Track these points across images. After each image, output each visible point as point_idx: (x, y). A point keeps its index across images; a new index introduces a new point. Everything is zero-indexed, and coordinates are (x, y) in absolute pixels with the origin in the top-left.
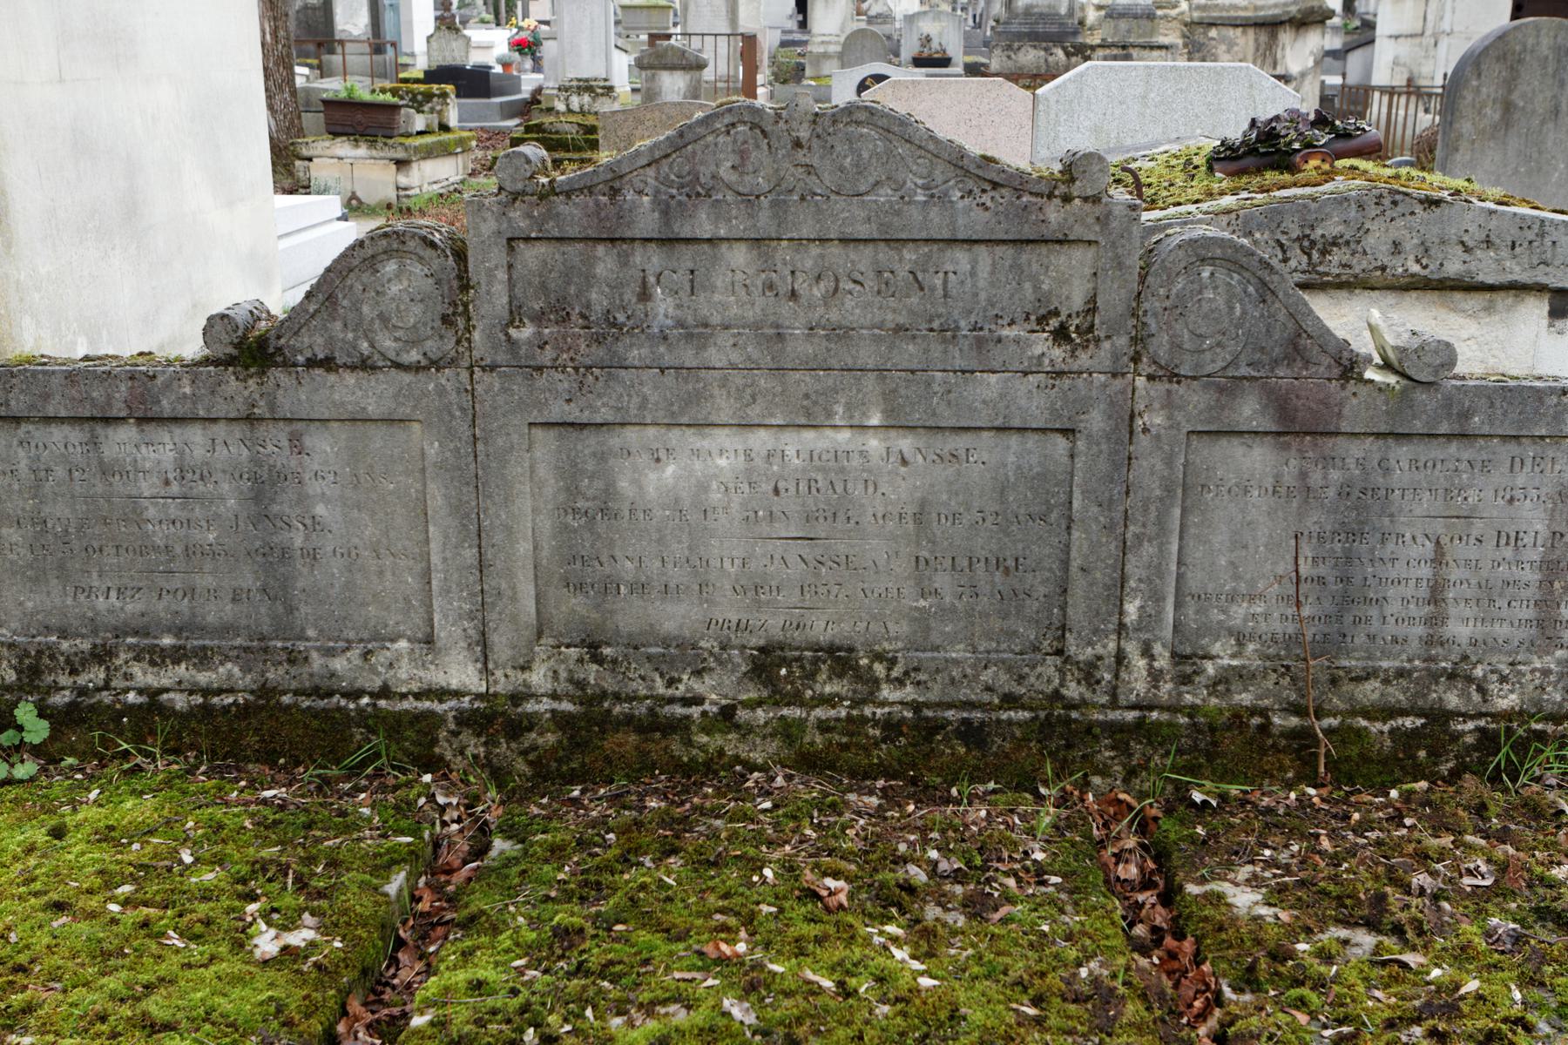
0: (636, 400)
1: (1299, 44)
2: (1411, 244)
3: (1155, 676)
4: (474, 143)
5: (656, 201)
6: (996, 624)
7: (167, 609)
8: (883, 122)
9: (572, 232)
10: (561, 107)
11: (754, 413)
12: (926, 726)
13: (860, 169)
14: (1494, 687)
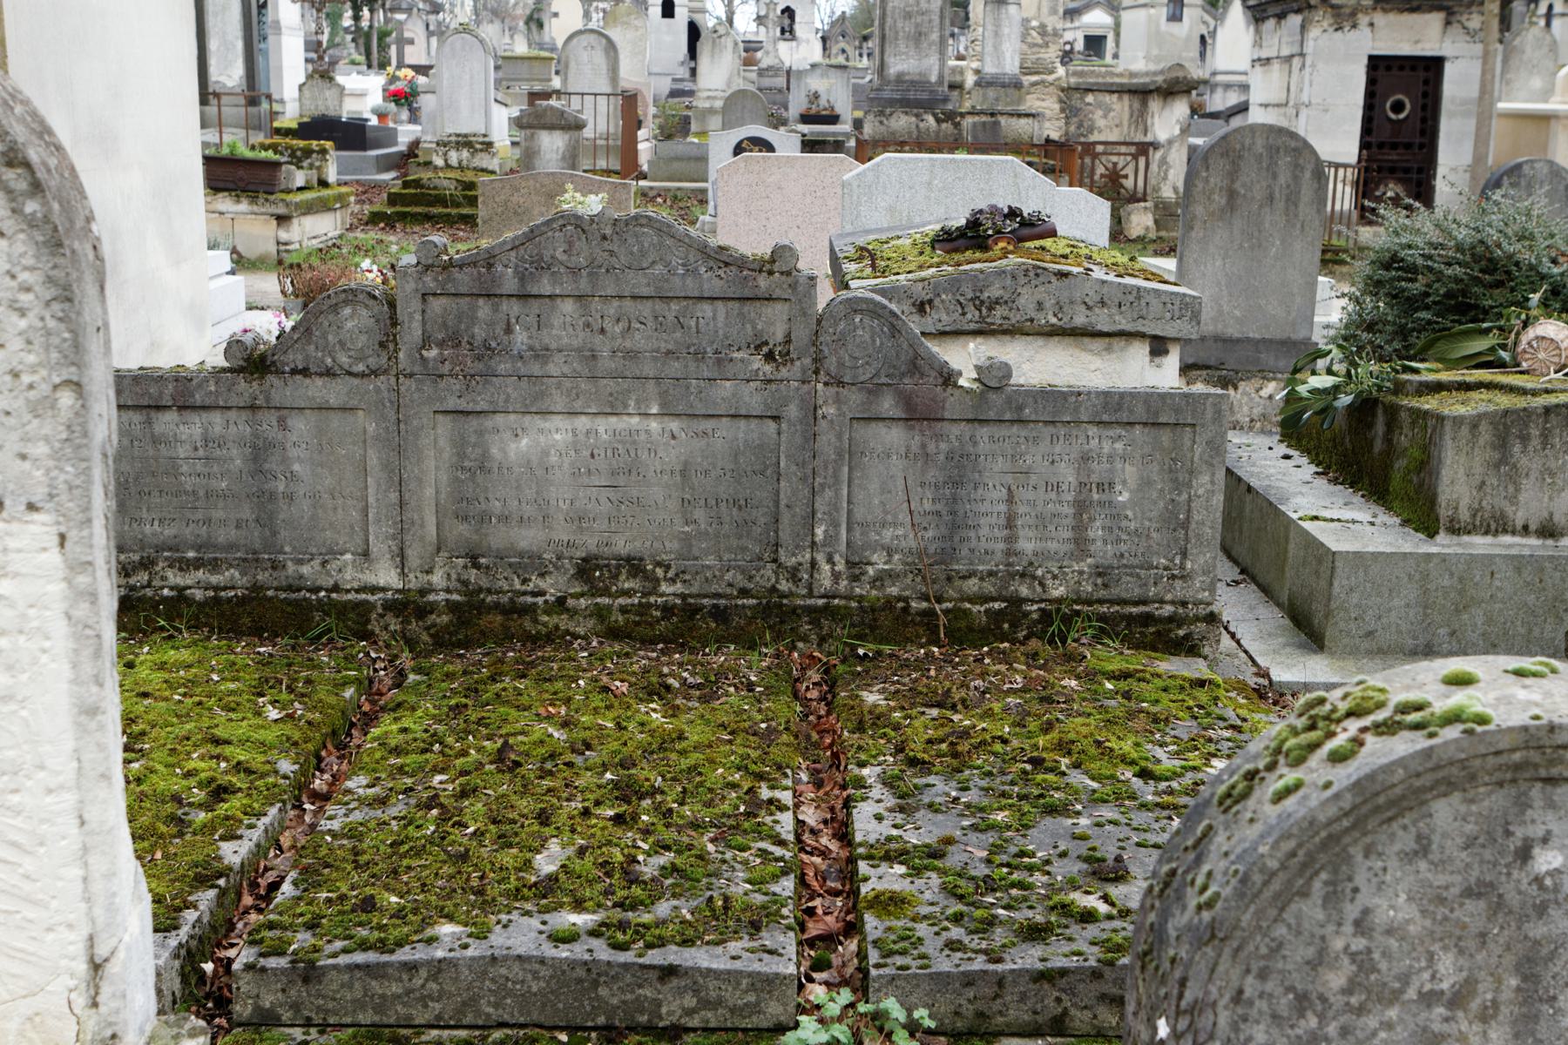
0: (503, 397)
1: (1166, 113)
2: (1049, 303)
3: (836, 576)
4: (352, 199)
5: (516, 272)
6: (735, 542)
7: (192, 533)
8: (657, 225)
9: (463, 290)
10: (439, 162)
11: (578, 405)
12: (688, 611)
13: (643, 253)
14: (1049, 582)
